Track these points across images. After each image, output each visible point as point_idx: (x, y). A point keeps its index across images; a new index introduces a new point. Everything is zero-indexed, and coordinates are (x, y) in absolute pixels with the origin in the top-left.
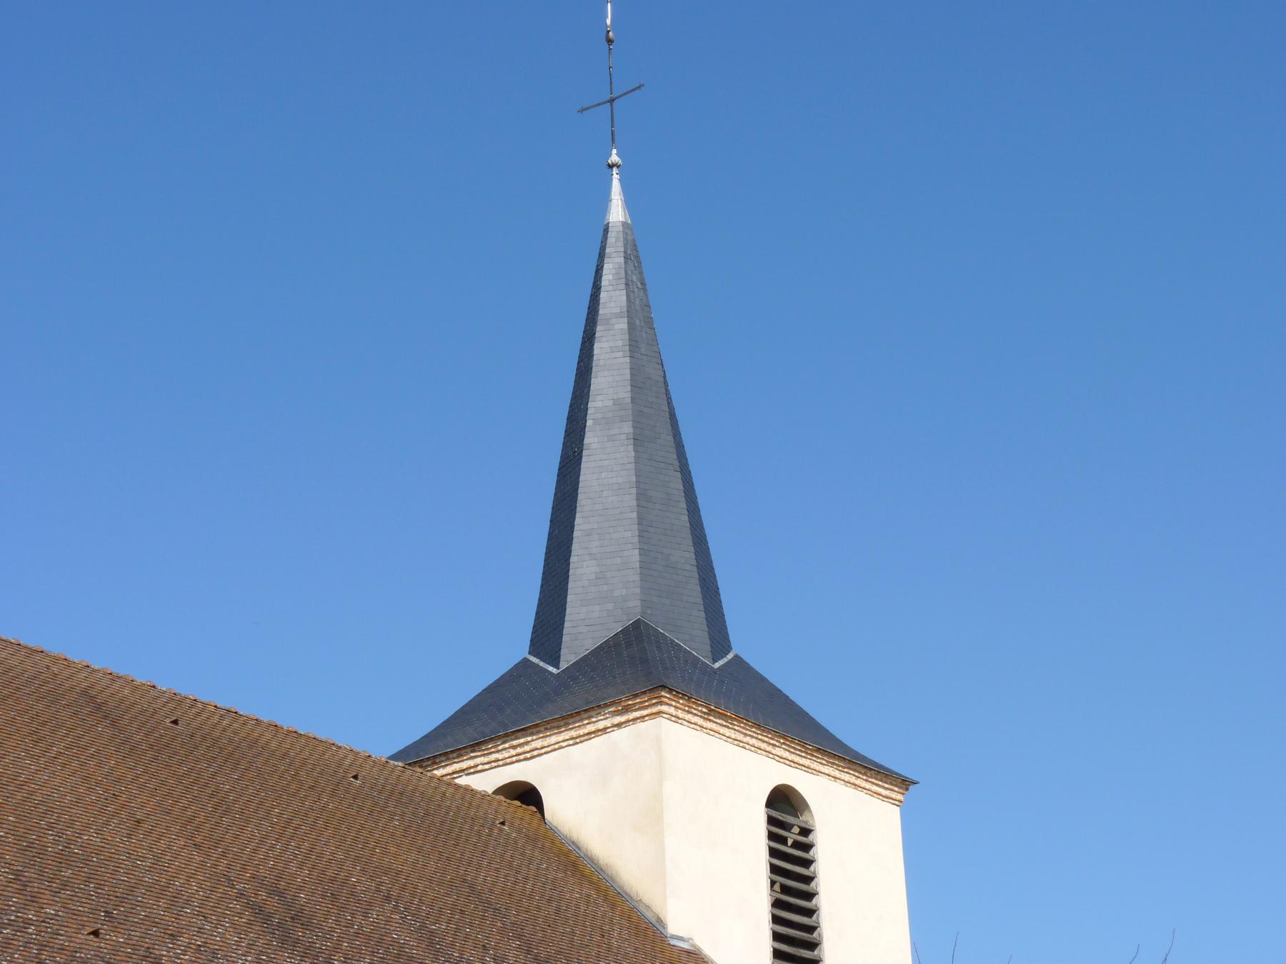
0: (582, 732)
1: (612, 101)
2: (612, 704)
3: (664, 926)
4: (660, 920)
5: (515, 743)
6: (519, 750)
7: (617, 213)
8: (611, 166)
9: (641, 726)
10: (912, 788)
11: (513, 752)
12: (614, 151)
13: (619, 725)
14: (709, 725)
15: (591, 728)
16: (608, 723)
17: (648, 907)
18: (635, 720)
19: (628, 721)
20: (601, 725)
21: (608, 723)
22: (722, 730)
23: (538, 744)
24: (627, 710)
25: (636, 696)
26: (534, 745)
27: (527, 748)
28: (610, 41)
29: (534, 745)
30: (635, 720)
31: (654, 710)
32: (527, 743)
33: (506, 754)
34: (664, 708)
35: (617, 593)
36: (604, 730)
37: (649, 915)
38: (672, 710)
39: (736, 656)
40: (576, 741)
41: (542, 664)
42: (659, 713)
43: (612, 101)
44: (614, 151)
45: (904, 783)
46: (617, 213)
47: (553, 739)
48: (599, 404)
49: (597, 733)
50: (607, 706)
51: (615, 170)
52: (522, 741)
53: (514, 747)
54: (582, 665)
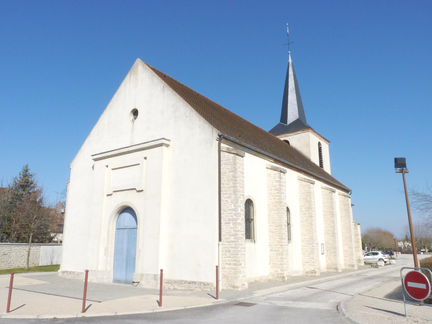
0: (296, 133)
1: (289, 44)
2: (301, 130)
3: (311, 160)
4: (310, 159)
5: (285, 135)
6: (285, 136)
7: (290, 61)
8: (289, 54)
9: (306, 133)
10: (330, 143)
11: (284, 136)
12: (289, 51)
13: (302, 133)
14: (313, 133)
15: (298, 133)
16: (300, 132)
17: (308, 157)
18: (305, 132)
19: (304, 132)
20: (299, 133)
21: (300, 132)
22: (314, 134)
23: (289, 135)
24: (304, 131)
25: (306, 129)
26: (288, 135)
27: (287, 135)
28: (288, 35)
29: (288, 135)
30: (305, 132)
31: (308, 131)
32: (287, 135)
33: (283, 136)
34: (310, 131)
35: (295, 115)
36: (300, 133)
37: (308, 158)
38: (310, 131)
39: (280, 122)
40: (295, 135)
41: (283, 124)
42: (309, 131)
43: (289, 44)
44: (289, 51)
45: (329, 142)
46: (290, 61)
47: (291, 134)
48: (290, 88)
49: (298, 134)
50: (301, 130)
51: (289, 54)
52: (286, 134)
53: (284, 135)
54: (291, 124)
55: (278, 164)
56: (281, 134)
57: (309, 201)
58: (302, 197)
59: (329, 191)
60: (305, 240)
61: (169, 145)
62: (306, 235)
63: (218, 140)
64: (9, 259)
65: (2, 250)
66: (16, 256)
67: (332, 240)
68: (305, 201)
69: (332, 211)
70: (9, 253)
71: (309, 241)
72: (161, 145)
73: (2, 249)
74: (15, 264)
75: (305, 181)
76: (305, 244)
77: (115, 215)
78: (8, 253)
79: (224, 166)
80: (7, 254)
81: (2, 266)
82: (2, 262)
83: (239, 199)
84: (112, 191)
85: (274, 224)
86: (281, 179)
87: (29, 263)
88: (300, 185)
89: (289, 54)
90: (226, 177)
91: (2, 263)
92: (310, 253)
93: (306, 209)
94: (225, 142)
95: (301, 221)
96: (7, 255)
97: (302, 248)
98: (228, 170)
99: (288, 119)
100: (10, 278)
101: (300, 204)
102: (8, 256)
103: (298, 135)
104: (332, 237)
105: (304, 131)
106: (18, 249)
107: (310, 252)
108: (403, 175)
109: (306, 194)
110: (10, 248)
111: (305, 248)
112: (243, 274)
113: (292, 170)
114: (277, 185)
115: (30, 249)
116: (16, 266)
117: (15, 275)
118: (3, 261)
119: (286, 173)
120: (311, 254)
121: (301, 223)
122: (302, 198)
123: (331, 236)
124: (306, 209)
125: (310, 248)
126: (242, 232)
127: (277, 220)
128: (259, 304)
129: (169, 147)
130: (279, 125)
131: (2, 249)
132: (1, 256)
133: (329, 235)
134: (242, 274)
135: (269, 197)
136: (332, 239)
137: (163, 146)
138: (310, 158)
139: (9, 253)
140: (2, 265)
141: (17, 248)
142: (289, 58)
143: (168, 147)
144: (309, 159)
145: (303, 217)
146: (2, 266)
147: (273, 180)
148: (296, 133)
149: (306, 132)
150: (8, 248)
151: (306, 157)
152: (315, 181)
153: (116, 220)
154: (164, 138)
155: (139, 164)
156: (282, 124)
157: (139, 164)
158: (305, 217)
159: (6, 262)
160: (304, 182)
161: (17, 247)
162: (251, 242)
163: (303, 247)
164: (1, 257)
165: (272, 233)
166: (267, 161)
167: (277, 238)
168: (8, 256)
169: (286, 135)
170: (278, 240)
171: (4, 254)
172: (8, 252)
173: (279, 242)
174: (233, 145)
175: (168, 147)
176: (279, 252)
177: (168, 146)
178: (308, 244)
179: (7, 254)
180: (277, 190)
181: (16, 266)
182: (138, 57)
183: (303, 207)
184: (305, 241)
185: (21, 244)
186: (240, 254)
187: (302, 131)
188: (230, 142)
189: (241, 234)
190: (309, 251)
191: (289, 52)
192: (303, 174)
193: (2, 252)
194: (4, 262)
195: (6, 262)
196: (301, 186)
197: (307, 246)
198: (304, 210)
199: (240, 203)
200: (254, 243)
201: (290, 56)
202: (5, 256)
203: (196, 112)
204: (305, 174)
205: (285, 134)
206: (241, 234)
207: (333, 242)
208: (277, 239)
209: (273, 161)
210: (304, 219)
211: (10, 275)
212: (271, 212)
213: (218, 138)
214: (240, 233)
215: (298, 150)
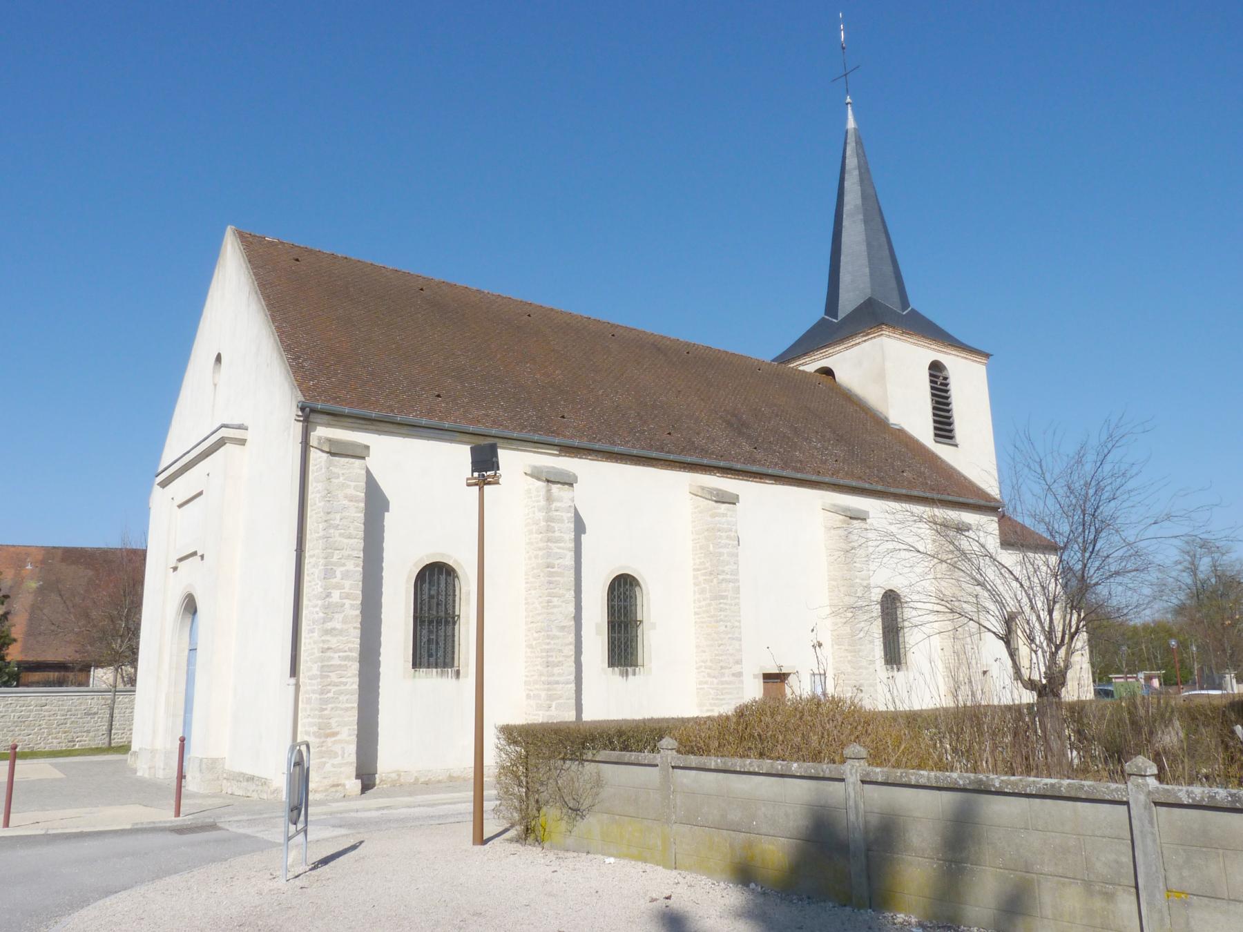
1: (846, 75)
4: (886, 418)
5: (821, 351)
6: (824, 354)
7: (851, 124)
9: (874, 340)
10: (991, 357)
11: (821, 355)
13: (865, 341)
15: (853, 343)
16: (860, 340)
17: (881, 413)
20: (857, 341)
21: (860, 340)
22: (908, 339)
24: (868, 334)
25: (871, 328)
27: (827, 353)
28: (843, 48)
33: (819, 356)
34: (884, 332)
36: (859, 343)
37: (882, 416)
40: (847, 349)
41: (830, 319)
42: (882, 334)
43: (846, 75)
45: (987, 356)
46: (851, 124)
47: (838, 349)
51: (849, 105)
52: (825, 350)
53: (821, 353)
55: (587, 459)
56: (812, 351)
57: (711, 553)
58: (698, 543)
59: (841, 517)
60: (703, 664)
61: (246, 440)
62: (704, 652)
63: (302, 419)
64: (103, 724)
65: (81, 703)
66: (122, 718)
67: (849, 662)
68: (703, 555)
69: (848, 577)
70: (101, 710)
71: (710, 668)
72: (221, 443)
73: (80, 701)
74: (120, 736)
75: (703, 496)
76: (704, 677)
77: (181, 616)
78: (100, 711)
79: (315, 484)
80: (95, 714)
81: (85, 741)
82: (84, 732)
83: (334, 568)
84: (175, 561)
85: (535, 625)
86: (553, 501)
87: (112, 735)
88: (695, 508)
89: (847, 104)
90: (316, 513)
91: (85, 734)
92: (713, 702)
93: (705, 576)
94: (332, 423)
95: (695, 612)
96: (97, 716)
97: (697, 689)
98: (318, 495)
99: (840, 302)
100: (7, 768)
101: (695, 564)
102: (99, 718)
103: (856, 348)
104: (848, 654)
105: (870, 337)
106: (127, 700)
107: (713, 699)
108: (481, 489)
109: (706, 533)
110: (103, 699)
111: (704, 688)
112: (343, 757)
113: (658, 470)
114: (541, 518)
115: (114, 701)
116: (124, 740)
117: (18, 762)
118: (86, 729)
119: (576, 483)
120: (715, 705)
121: (697, 616)
122: (698, 545)
123: (847, 650)
124: (704, 578)
125: (712, 689)
126: (345, 651)
127: (539, 614)
128: (230, 829)
129: (246, 444)
130: (822, 322)
131: (80, 701)
132: (81, 718)
133: (843, 647)
134: (340, 758)
135: (528, 553)
136: (849, 658)
137: (225, 443)
138: (887, 416)
139: (103, 711)
140: (84, 738)
141: (123, 698)
142: (846, 118)
143: (244, 445)
144: (883, 418)
145: (700, 602)
146: (85, 741)
147: (534, 507)
148: (849, 345)
149: (874, 337)
150: (98, 699)
151: (878, 413)
152: (738, 495)
153: (187, 629)
154: (225, 423)
155: (200, 494)
156: (828, 320)
157: (200, 494)
158: (704, 600)
159: (94, 731)
160: (702, 499)
161: (122, 697)
162: (442, 676)
163: (699, 684)
164: (81, 720)
165: (530, 650)
166: (532, 454)
167: (537, 663)
168: (99, 718)
169: (824, 352)
170: (539, 667)
171: (87, 714)
172: (98, 709)
173: (541, 675)
174: (367, 427)
175: (244, 445)
176: (540, 702)
177: (242, 442)
178: (709, 675)
179: (95, 714)
180: (541, 533)
181: (125, 742)
182: (228, 224)
183: (699, 572)
184: (703, 669)
185: (14, 691)
186: (329, 709)
187: (864, 336)
188: (349, 420)
189: (339, 657)
190: (711, 697)
191: (849, 100)
192: (718, 475)
193: (83, 707)
194: (88, 731)
195: (94, 731)
196: (695, 513)
197: (706, 683)
198: (701, 578)
199: (342, 579)
200: (454, 679)
201: (852, 110)
202: (91, 718)
203: (275, 355)
204: (729, 476)
205: (822, 348)
206: (339, 657)
207: (852, 667)
208: (537, 665)
209: (558, 453)
210: (701, 604)
211: (7, 763)
212: (530, 594)
213: (298, 416)
214: (336, 655)
215: (856, 395)
